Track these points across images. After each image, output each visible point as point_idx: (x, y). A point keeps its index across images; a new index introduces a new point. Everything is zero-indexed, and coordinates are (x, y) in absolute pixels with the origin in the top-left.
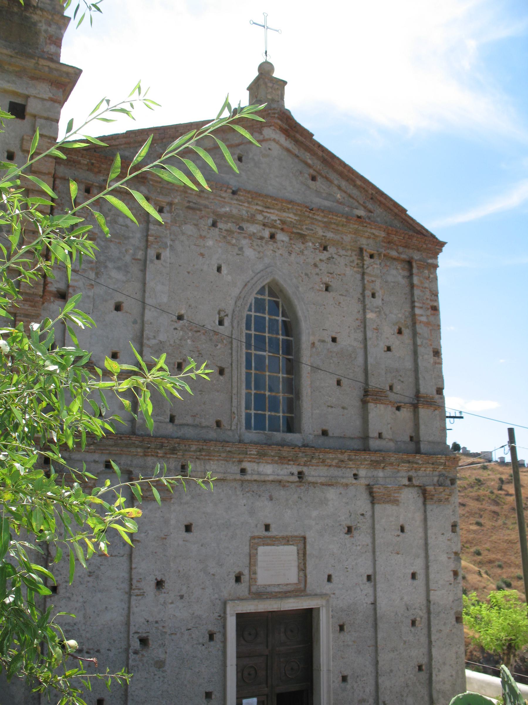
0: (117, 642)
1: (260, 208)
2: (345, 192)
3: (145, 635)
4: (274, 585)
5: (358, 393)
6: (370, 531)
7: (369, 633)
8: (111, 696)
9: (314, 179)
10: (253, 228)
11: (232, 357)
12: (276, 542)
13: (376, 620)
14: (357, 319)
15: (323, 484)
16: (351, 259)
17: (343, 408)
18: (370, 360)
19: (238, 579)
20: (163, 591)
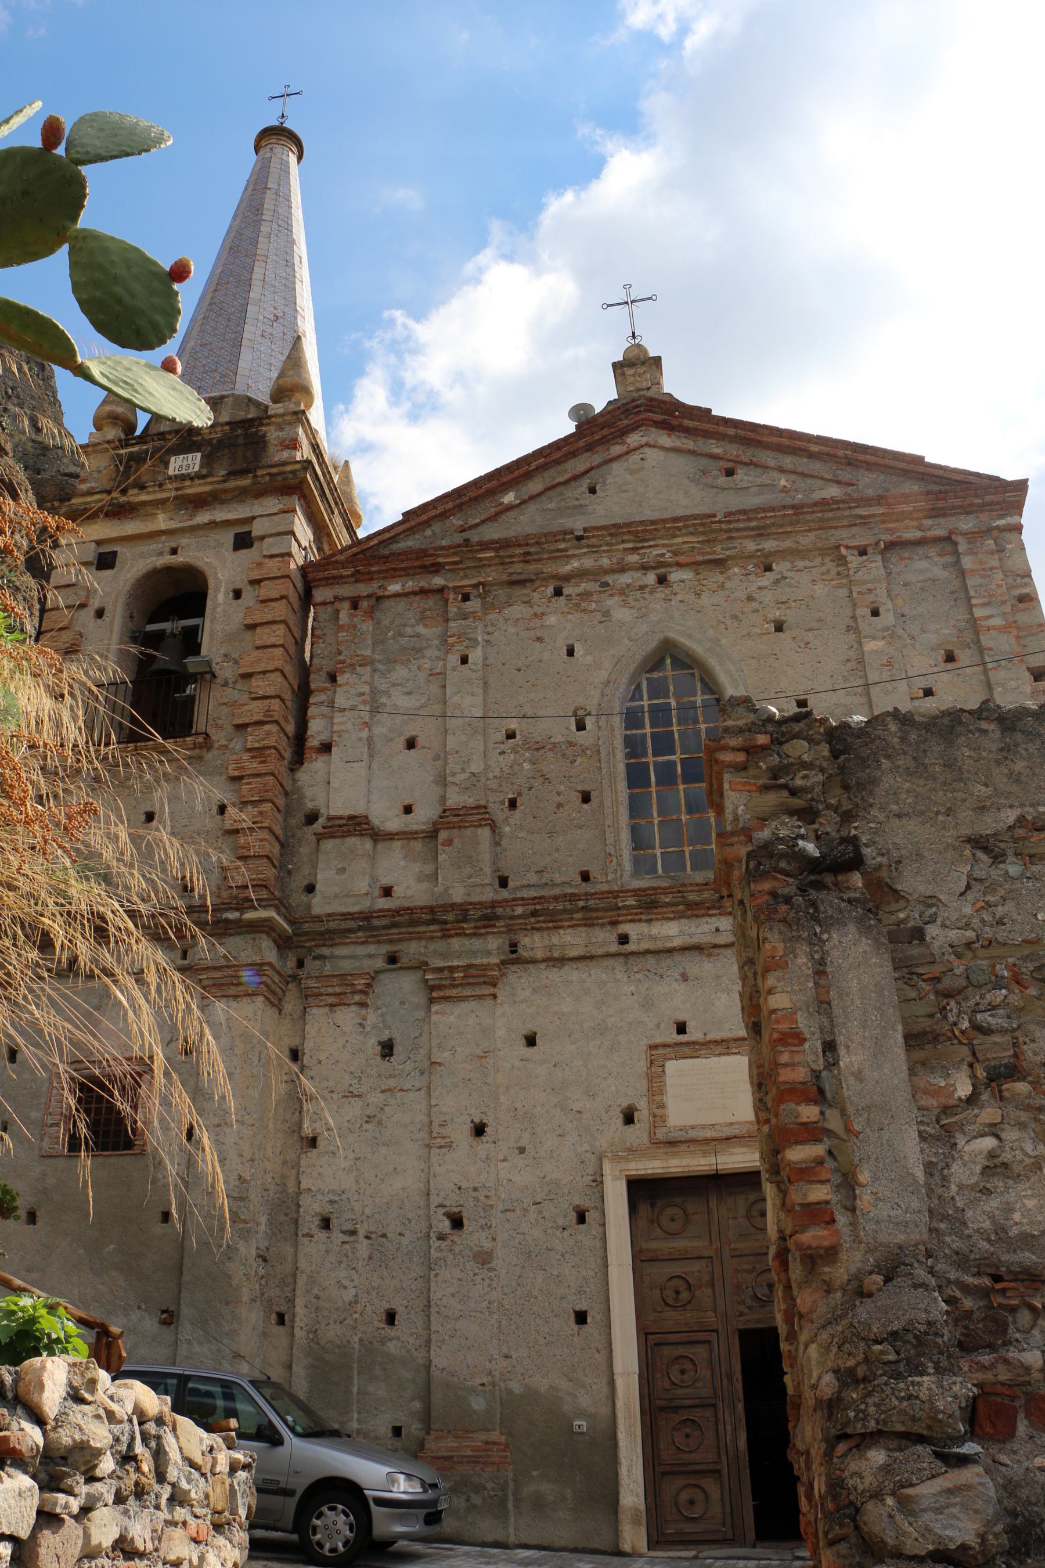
0: (413, 1221)
1: (630, 545)
2: (794, 472)
4: (703, 1127)
8: (406, 1307)
9: (730, 473)
12: (702, 1052)
16: (824, 569)
19: (629, 1118)
20: (483, 1138)
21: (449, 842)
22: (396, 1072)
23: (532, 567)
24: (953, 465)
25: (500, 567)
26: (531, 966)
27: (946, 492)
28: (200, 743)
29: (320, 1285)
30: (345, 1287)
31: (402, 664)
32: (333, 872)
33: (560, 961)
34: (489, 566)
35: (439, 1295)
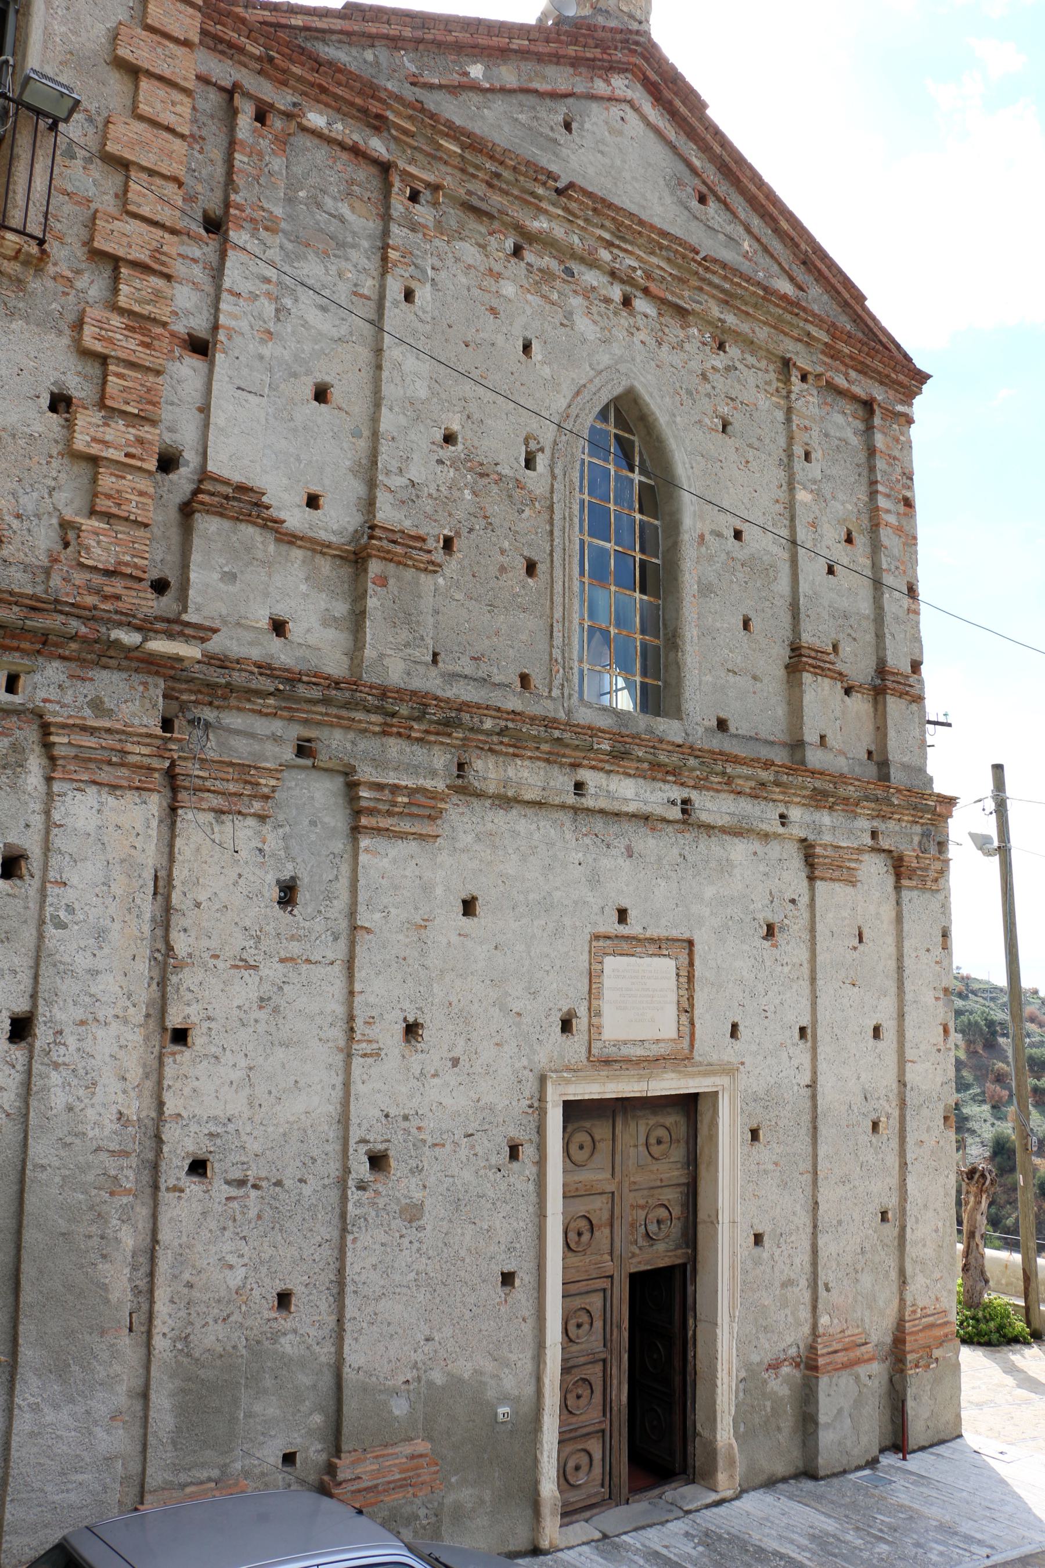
0: (319, 1161)
1: (607, 236)
2: (758, 240)
3: (381, 1147)
4: (634, 1043)
5: (781, 653)
6: (806, 936)
7: (803, 1145)
9: (702, 200)
10: (591, 278)
11: (552, 541)
12: (638, 950)
13: (815, 1118)
14: (777, 501)
15: (724, 830)
16: (767, 377)
17: (755, 678)
18: (804, 587)
19: (566, 1026)
21: (382, 581)
22: (301, 932)
23: (497, 200)
24: (885, 323)
25: (458, 174)
26: (473, 799)
27: (877, 352)
28: (29, 254)
29: (194, 1267)
30: (231, 1267)
31: (317, 254)
32: (216, 576)
33: (506, 801)
34: (446, 163)
35: (357, 1268)
